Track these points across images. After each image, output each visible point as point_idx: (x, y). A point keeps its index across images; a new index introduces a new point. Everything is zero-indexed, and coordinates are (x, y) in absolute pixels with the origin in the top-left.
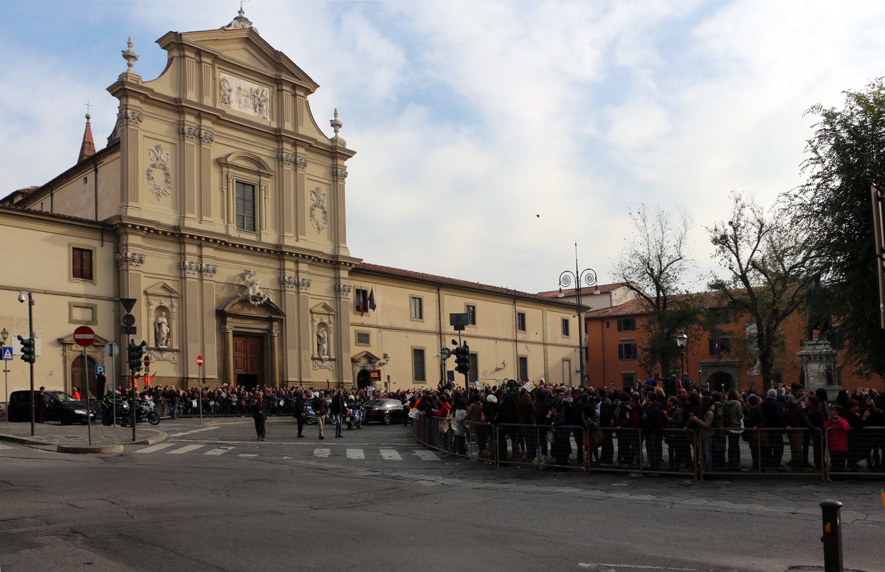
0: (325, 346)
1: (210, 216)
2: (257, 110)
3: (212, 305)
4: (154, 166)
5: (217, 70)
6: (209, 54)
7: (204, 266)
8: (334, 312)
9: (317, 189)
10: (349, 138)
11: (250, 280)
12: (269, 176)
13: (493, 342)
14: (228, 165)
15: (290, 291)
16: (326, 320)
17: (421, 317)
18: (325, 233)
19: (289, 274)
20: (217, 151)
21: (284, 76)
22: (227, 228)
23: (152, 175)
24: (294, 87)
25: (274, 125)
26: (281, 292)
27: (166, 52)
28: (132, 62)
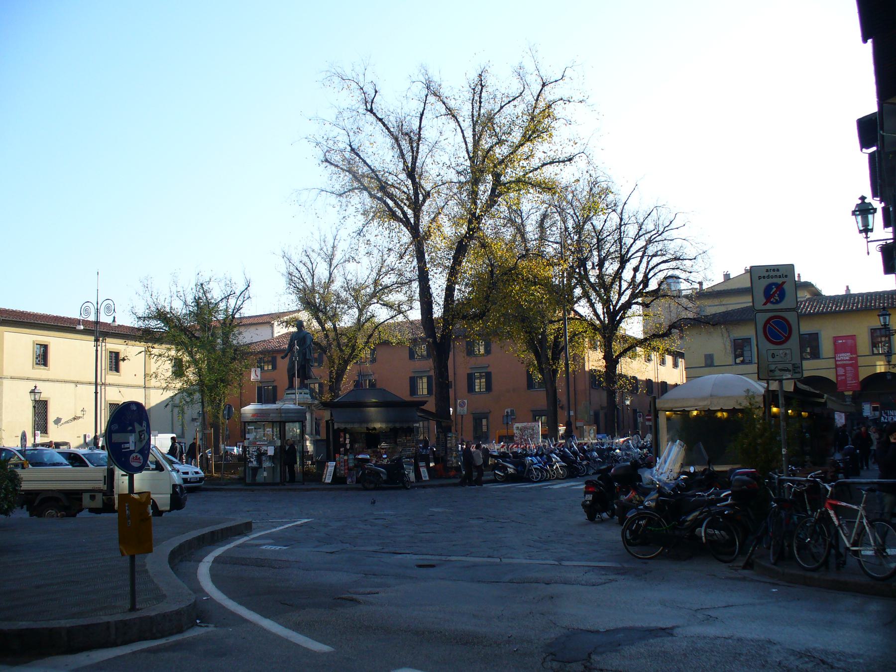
13: (73, 385)
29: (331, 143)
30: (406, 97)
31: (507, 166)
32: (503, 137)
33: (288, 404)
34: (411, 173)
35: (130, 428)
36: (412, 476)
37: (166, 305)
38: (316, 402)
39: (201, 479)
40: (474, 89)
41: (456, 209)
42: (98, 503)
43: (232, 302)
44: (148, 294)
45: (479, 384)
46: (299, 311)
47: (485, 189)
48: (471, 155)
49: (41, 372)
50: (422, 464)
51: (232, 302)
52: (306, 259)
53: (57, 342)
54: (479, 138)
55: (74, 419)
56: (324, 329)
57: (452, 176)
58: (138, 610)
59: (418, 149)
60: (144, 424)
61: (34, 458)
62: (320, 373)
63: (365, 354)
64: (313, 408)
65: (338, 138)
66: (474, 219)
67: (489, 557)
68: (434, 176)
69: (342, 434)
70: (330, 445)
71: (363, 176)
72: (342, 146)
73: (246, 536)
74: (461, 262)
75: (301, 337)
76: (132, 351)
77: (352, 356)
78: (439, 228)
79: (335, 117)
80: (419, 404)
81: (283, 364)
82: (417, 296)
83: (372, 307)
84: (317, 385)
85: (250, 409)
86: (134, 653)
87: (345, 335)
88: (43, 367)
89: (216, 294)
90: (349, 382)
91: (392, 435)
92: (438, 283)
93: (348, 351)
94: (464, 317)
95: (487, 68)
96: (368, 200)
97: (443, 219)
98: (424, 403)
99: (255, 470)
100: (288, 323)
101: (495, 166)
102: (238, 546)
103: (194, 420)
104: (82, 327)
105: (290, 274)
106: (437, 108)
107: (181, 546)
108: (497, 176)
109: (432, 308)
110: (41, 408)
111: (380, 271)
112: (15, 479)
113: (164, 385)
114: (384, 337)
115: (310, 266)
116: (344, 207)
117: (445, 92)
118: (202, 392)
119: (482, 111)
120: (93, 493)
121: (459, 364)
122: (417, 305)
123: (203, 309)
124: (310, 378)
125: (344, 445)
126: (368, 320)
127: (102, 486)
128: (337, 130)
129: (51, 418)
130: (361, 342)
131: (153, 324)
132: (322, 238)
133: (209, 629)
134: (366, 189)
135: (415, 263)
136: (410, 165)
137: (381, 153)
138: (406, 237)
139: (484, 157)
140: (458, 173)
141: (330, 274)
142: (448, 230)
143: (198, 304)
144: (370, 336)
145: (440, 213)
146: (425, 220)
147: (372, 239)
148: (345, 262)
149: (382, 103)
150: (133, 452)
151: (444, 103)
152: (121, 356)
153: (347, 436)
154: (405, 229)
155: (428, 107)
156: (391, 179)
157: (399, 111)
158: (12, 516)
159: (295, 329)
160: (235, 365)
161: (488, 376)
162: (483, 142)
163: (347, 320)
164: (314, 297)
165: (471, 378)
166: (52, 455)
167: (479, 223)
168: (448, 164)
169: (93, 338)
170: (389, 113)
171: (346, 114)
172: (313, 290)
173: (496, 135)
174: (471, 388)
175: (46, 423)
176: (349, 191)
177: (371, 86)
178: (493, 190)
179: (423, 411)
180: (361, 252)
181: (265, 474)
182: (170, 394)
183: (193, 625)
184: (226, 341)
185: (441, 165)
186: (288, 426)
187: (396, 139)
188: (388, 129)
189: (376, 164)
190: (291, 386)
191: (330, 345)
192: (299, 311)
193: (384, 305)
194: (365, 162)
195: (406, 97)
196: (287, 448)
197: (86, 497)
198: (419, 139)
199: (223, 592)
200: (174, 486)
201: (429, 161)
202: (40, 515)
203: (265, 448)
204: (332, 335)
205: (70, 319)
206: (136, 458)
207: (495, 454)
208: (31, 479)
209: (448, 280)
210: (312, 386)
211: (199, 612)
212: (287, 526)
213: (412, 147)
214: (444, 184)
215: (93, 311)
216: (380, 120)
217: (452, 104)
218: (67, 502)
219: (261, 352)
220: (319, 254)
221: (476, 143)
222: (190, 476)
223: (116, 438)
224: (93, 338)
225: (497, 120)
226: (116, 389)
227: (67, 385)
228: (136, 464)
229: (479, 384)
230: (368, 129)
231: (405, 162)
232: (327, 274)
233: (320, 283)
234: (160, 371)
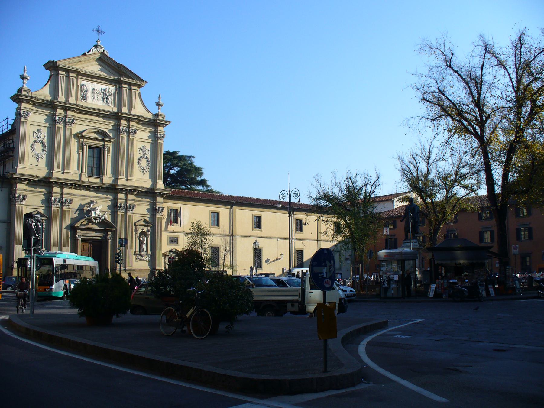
0: (144, 246)
1: (24, 164)
2: (105, 101)
3: (67, 222)
4: (35, 141)
5: (80, 80)
6: (73, 71)
7: (64, 200)
8: (152, 223)
9: (143, 147)
10: (166, 113)
11: (94, 207)
12: (110, 141)
13: (275, 240)
14: (83, 137)
15: (121, 213)
16: (145, 230)
17: (218, 226)
18: (147, 175)
19: (121, 202)
20: (76, 129)
21: (124, 79)
22: (80, 176)
23: (34, 146)
24: (130, 84)
25: (115, 110)
26: (114, 214)
27: (48, 72)
28: (160, 107)
29: (426, 88)
30: (472, 56)
31: (540, 95)
32: (537, 76)
33: (407, 248)
34: (478, 103)
35: (324, 264)
36: (484, 293)
37: (329, 191)
38: (422, 247)
39: (354, 295)
40: (516, 47)
41: (507, 124)
42: (296, 309)
43: (369, 188)
44: (318, 185)
45: (524, 235)
46: (409, 192)
47: (526, 111)
48: (516, 89)
49: (257, 232)
50: (490, 286)
51: (369, 188)
52: (413, 160)
53: (267, 215)
54: (521, 78)
55: (277, 259)
56: (425, 203)
57: (502, 103)
58: (328, 372)
59: (481, 88)
60: (332, 261)
61: (257, 281)
62: (424, 230)
63: (451, 217)
64: (421, 251)
65: (431, 85)
66: (519, 131)
67: (542, 346)
68: (492, 104)
69: (440, 267)
70: (432, 276)
71: (447, 107)
72: (433, 89)
73: (384, 329)
74: (512, 158)
75: (412, 206)
76: (310, 219)
77: (443, 219)
78: (496, 137)
79: (428, 72)
80: (487, 248)
81: (401, 225)
82: (484, 180)
83: (455, 188)
84: (421, 238)
85: (383, 252)
86: (328, 397)
87: (439, 206)
88: (258, 229)
89: (359, 183)
90: (441, 235)
91: (471, 267)
92: (497, 172)
93: (440, 216)
94: (515, 193)
95: (524, 32)
96: (451, 122)
97: (499, 132)
98: (491, 247)
99: (386, 290)
100: (403, 200)
101: (532, 95)
102: (381, 335)
103: (347, 259)
104: (281, 206)
105: (404, 170)
106: (492, 61)
107: (347, 335)
108: (534, 102)
109: (494, 188)
110: (258, 253)
111: (459, 166)
112: (251, 294)
113: (331, 239)
114: (463, 206)
115: (415, 164)
116: (436, 127)
117: (497, 50)
118: (354, 243)
119: (522, 60)
120: (293, 302)
121: (512, 222)
122: (485, 186)
123: (352, 192)
124: (418, 233)
125: (441, 274)
126: (452, 196)
127: (298, 298)
128: (430, 80)
129: (264, 259)
130: (448, 210)
131: (323, 203)
132: (422, 147)
133: (370, 385)
134: (449, 115)
135: (482, 160)
136: (476, 99)
137: (458, 92)
138: (476, 143)
139: (525, 91)
140: (508, 101)
141: (428, 169)
142: (502, 138)
143: (348, 190)
144: (454, 206)
145: (496, 128)
146: (487, 132)
147: (455, 146)
148: (437, 161)
149: (457, 61)
150: (325, 278)
151: (496, 58)
152: (304, 222)
153: (443, 268)
154: (474, 138)
155: (486, 60)
156: (465, 108)
157: (467, 65)
158: (251, 315)
159: (406, 204)
160: (372, 226)
161: (530, 230)
162: (524, 80)
163: (440, 197)
164: (419, 183)
165: (518, 231)
166: (267, 280)
167: (523, 133)
168: (501, 96)
169: (287, 212)
170: (461, 67)
171: (435, 70)
172: (418, 179)
173: (533, 75)
174: (519, 237)
175: (261, 262)
176: (439, 117)
177: (449, 51)
178: (532, 111)
179: (491, 252)
180: (447, 153)
181: (393, 292)
182: (334, 244)
183: (360, 382)
184: (365, 213)
185: (496, 97)
186: (406, 262)
187: (467, 83)
188: (461, 77)
189: (455, 100)
190: (407, 238)
191: (429, 212)
192: (409, 192)
193: (462, 187)
194: (448, 98)
195: (472, 56)
196: (406, 276)
197: (289, 305)
198: (482, 82)
199: (375, 363)
200: (341, 299)
201: (488, 95)
202: (263, 315)
203: (392, 276)
204: (430, 206)
205: (273, 201)
206: (327, 282)
207: (538, 280)
208: (258, 294)
209: (504, 170)
210: (418, 238)
211: (363, 375)
212: (409, 324)
213: (477, 87)
214: (498, 109)
215: (287, 196)
216: (456, 72)
217: (502, 57)
218: (277, 308)
219: (387, 218)
220: (421, 157)
221: (519, 81)
222: (348, 293)
223: (316, 270)
224: (287, 212)
225: (532, 65)
226: (300, 242)
227: (273, 240)
228: (327, 286)
229: (524, 235)
230: (449, 78)
231: (473, 97)
232: (426, 169)
233: (422, 174)
234: (328, 230)
